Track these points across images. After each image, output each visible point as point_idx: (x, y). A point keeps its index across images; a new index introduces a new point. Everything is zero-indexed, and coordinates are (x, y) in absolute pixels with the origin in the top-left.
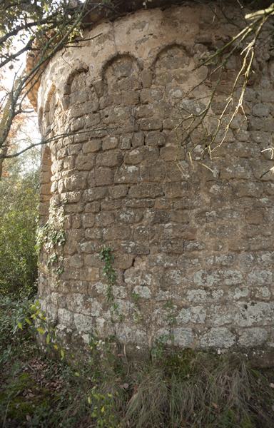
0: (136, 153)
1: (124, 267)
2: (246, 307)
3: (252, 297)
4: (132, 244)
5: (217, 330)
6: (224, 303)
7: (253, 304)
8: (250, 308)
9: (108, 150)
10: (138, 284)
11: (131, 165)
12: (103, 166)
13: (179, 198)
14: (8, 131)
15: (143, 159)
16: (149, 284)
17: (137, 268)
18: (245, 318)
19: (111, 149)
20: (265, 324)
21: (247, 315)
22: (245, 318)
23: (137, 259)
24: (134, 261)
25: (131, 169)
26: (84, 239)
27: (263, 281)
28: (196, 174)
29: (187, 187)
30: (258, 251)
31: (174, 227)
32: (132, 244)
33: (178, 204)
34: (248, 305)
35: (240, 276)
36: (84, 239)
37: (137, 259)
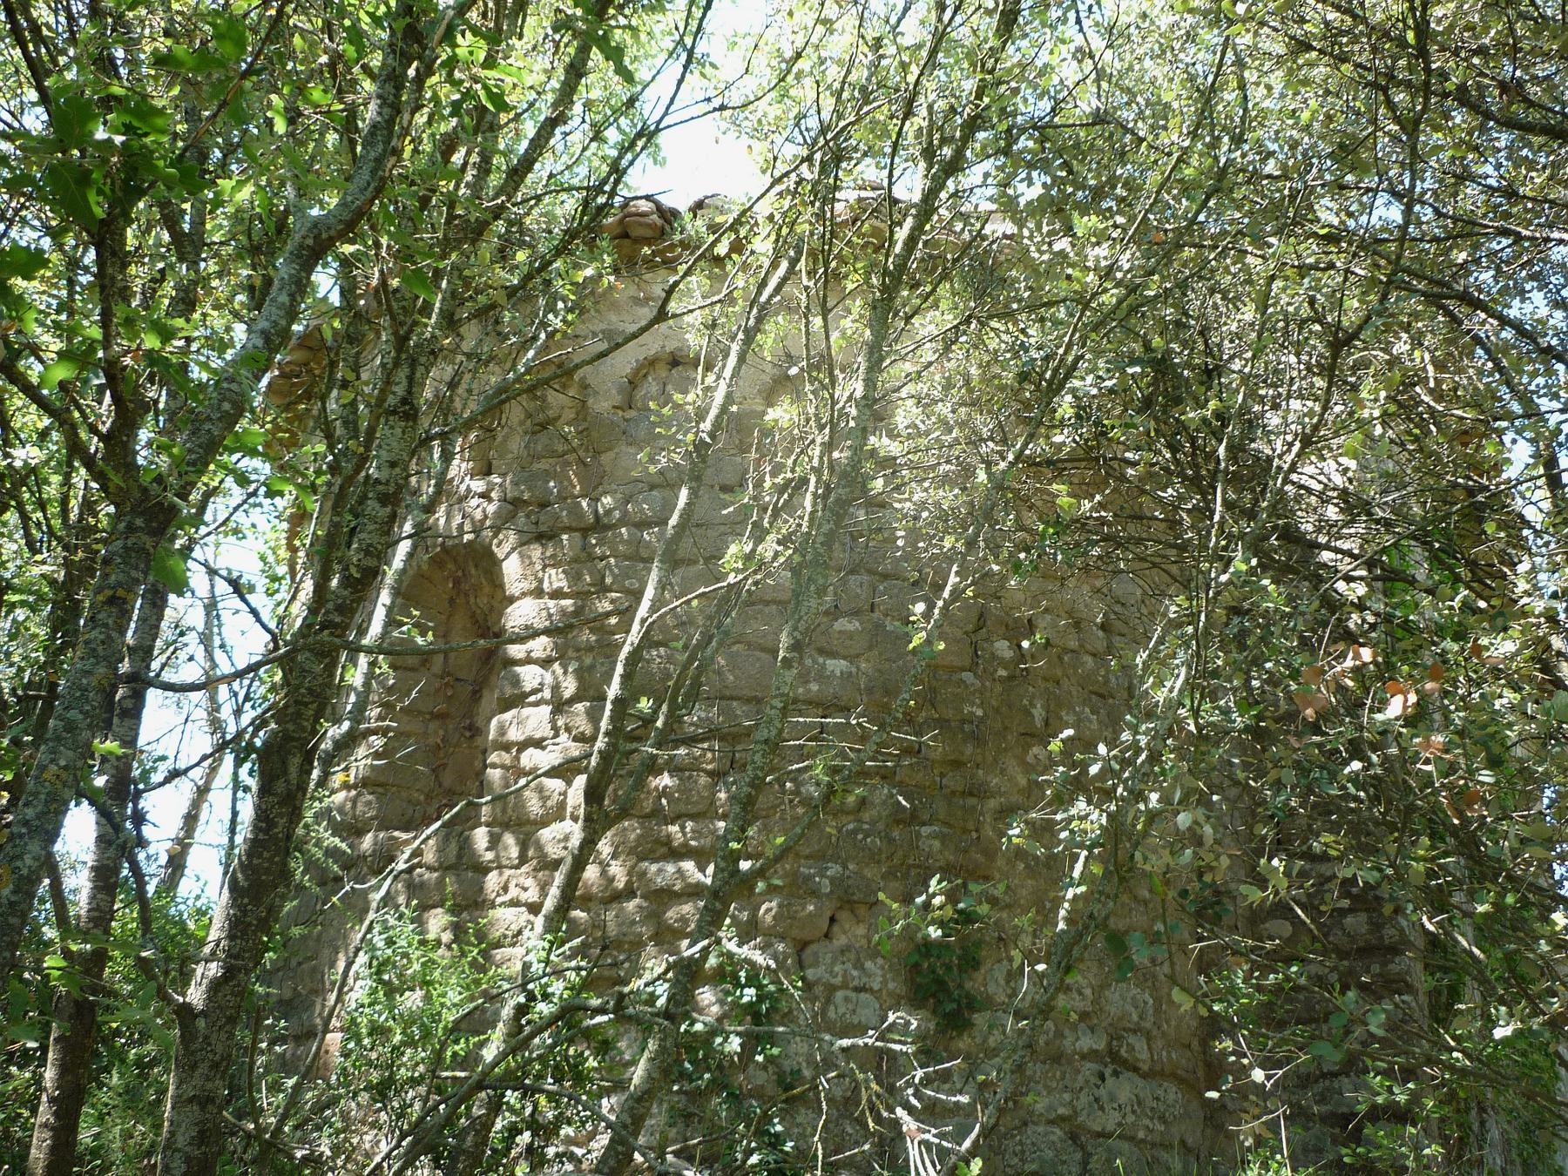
0: (850, 627)
1: (805, 935)
2: (1102, 1078)
3: (1113, 1055)
4: (834, 870)
5: (1041, 1129)
6: (1057, 1058)
7: (1116, 1074)
8: (1110, 1081)
9: (767, 603)
10: (845, 986)
11: (833, 655)
12: (749, 644)
13: (957, 764)
14: (870, 370)
15: (870, 648)
16: (876, 987)
17: (841, 940)
18: (1102, 1108)
19: (774, 602)
20: (1141, 1135)
21: (1105, 1098)
22: (1102, 1108)
23: (844, 916)
24: (832, 920)
25: (836, 666)
26: (664, 850)
27: (1135, 1017)
28: (997, 711)
29: (977, 739)
30: (1246, 110)
31: (943, 838)
32: (834, 870)
33: (954, 781)
34: (1108, 1072)
35: (1088, 992)
36: (664, 850)
37: (844, 916)
